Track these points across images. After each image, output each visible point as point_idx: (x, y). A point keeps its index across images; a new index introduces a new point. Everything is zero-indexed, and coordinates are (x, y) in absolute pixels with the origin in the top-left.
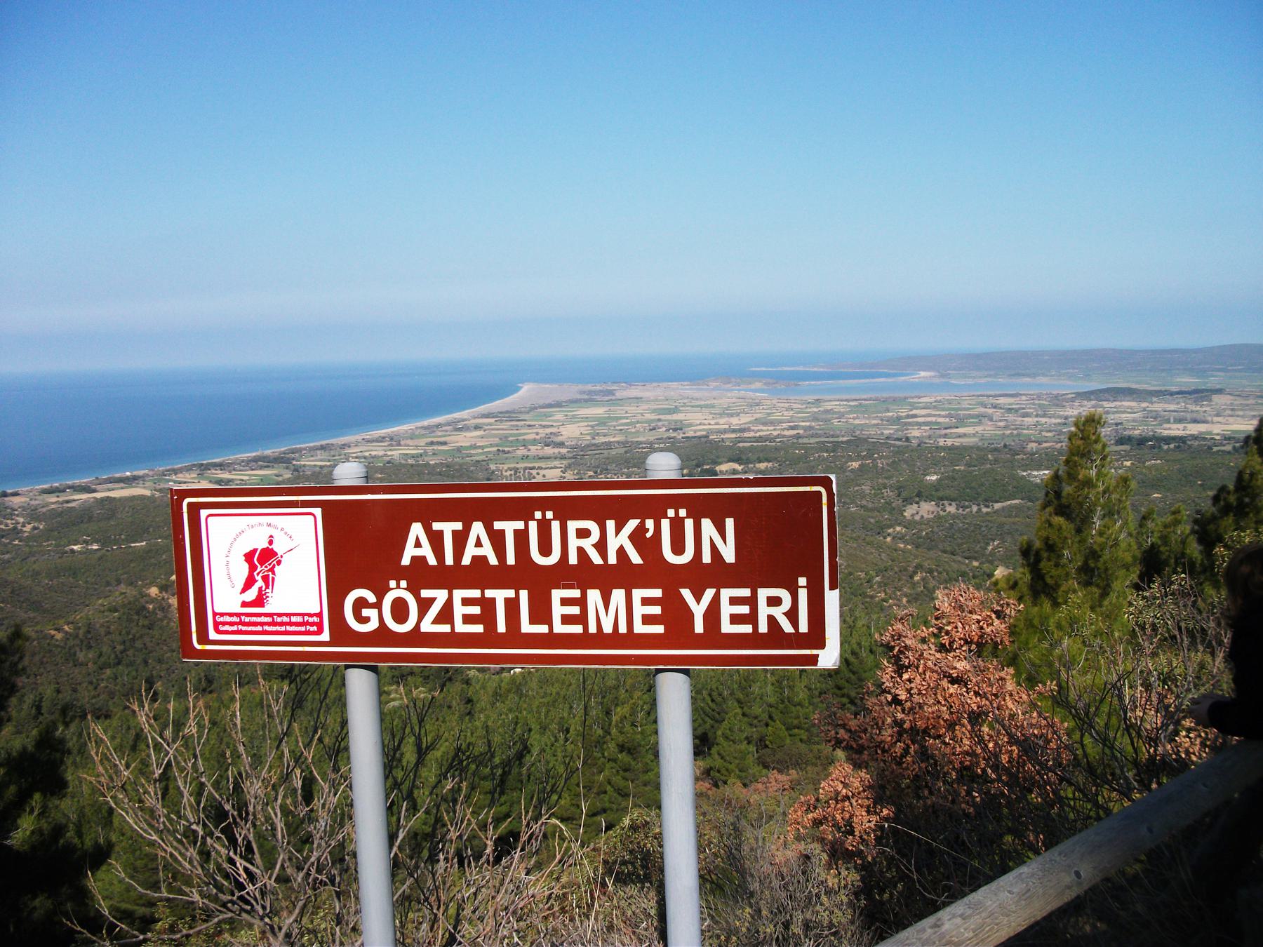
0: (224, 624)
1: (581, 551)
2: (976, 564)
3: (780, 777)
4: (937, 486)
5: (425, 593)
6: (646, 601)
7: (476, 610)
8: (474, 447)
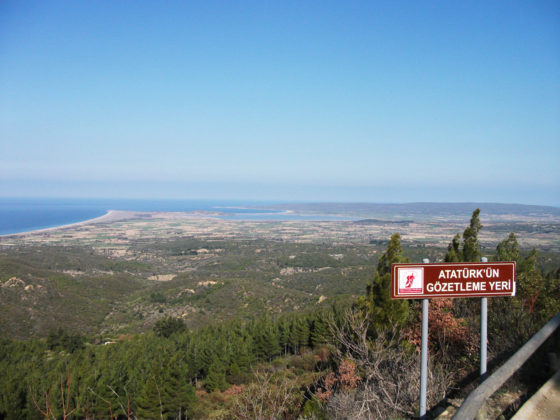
1: (472, 275)
2: (311, 294)
3: (237, 387)
4: (294, 261)
5: (443, 284)
6: (483, 284)
7: (452, 287)
8: (85, 239)
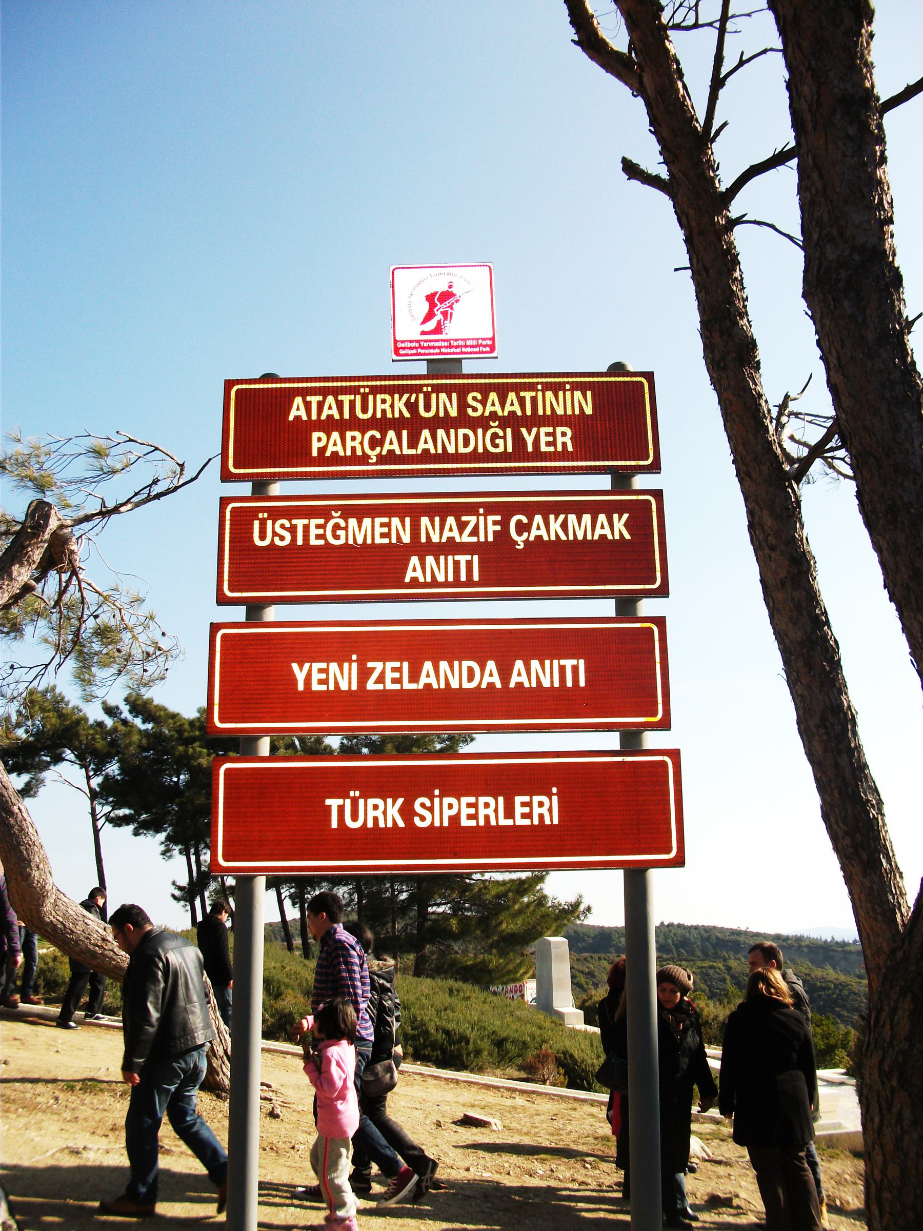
0: (404, 348)
